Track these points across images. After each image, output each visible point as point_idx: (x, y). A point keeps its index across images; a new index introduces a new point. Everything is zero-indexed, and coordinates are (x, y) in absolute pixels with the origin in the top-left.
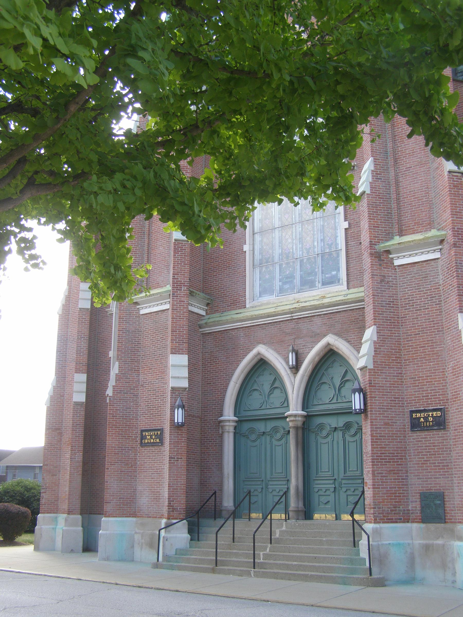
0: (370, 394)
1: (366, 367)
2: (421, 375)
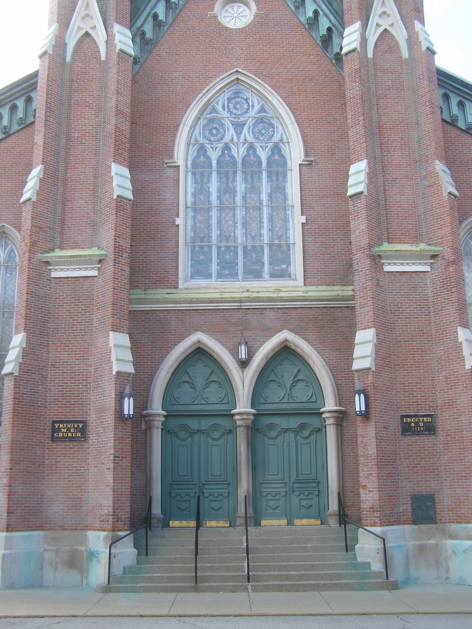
2: (411, 382)
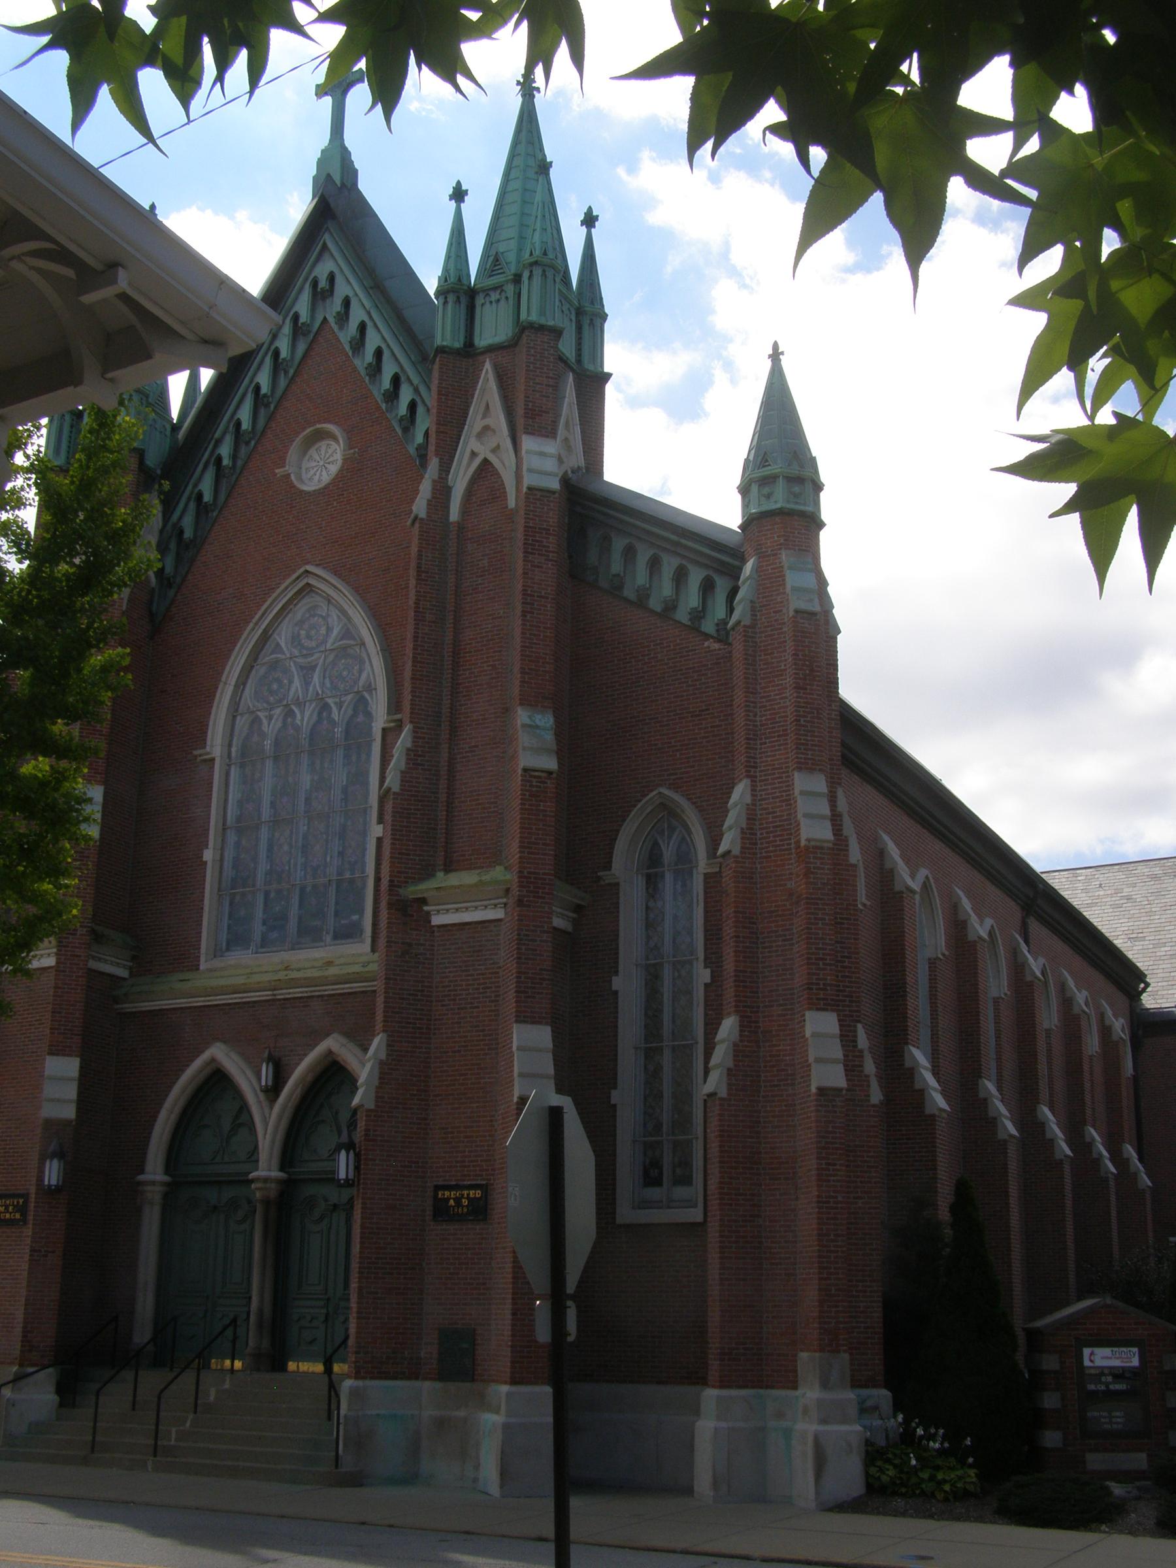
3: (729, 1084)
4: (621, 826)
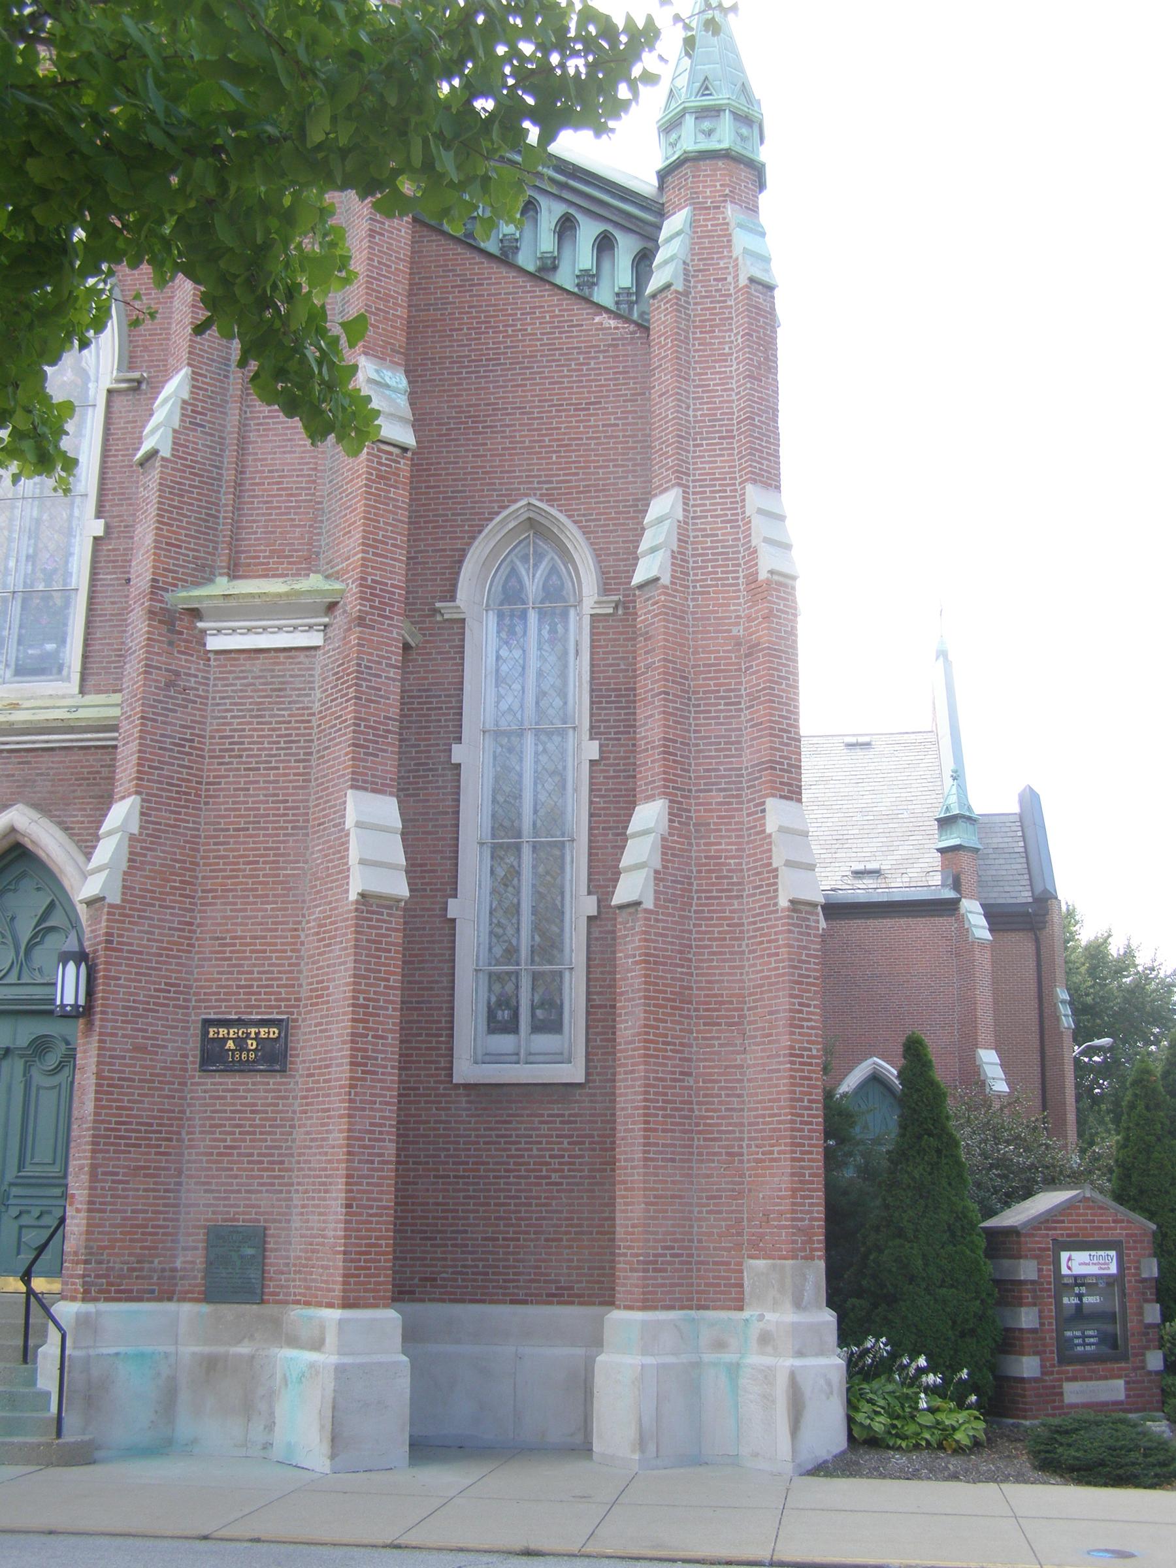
0: (105, 970)
1: (103, 899)
3: (656, 892)
4: (470, 544)
